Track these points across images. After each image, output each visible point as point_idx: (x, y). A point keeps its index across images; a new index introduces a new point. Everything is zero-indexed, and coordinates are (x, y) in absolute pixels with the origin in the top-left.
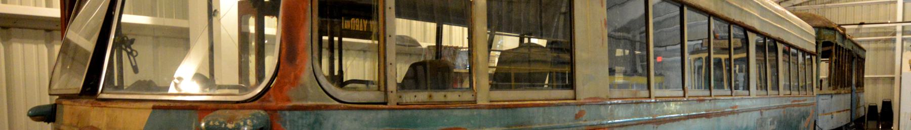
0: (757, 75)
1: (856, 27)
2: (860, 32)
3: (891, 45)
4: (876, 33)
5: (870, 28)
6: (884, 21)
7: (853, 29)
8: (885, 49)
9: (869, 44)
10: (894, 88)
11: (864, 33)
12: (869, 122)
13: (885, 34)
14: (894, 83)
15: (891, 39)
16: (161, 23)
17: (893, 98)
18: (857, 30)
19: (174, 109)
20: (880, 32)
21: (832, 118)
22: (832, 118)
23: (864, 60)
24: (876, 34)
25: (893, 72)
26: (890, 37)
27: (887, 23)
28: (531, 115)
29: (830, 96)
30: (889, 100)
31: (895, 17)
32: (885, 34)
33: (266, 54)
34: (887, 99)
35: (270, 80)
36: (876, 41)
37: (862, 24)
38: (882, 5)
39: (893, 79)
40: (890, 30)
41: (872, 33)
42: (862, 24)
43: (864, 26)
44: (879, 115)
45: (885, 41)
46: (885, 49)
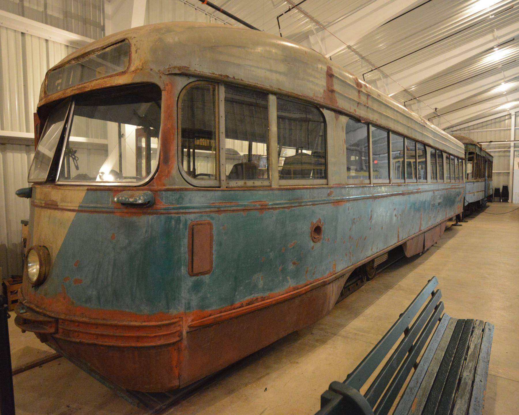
1: (488, 143)
2: (490, 146)
3: (508, 154)
5: (495, 144)
7: (486, 145)
8: (504, 156)
10: (509, 178)
13: (504, 147)
17: (509, 184)
18: (489, 145)
20: (501, 147)
24: (499, 148)
25: (509, 169)
26: (507, 149)
31: (510, 138)
32: (504, 147)
33: (151, 159)
34: (505, 184)
36: (499, 152)
37: (491, 142)
39: (509, 173)
41: (497, 147)
42: (491, 142)
43: (492, 143)
44: (501, 194)
45: (505, 151)
46: (504, 156)
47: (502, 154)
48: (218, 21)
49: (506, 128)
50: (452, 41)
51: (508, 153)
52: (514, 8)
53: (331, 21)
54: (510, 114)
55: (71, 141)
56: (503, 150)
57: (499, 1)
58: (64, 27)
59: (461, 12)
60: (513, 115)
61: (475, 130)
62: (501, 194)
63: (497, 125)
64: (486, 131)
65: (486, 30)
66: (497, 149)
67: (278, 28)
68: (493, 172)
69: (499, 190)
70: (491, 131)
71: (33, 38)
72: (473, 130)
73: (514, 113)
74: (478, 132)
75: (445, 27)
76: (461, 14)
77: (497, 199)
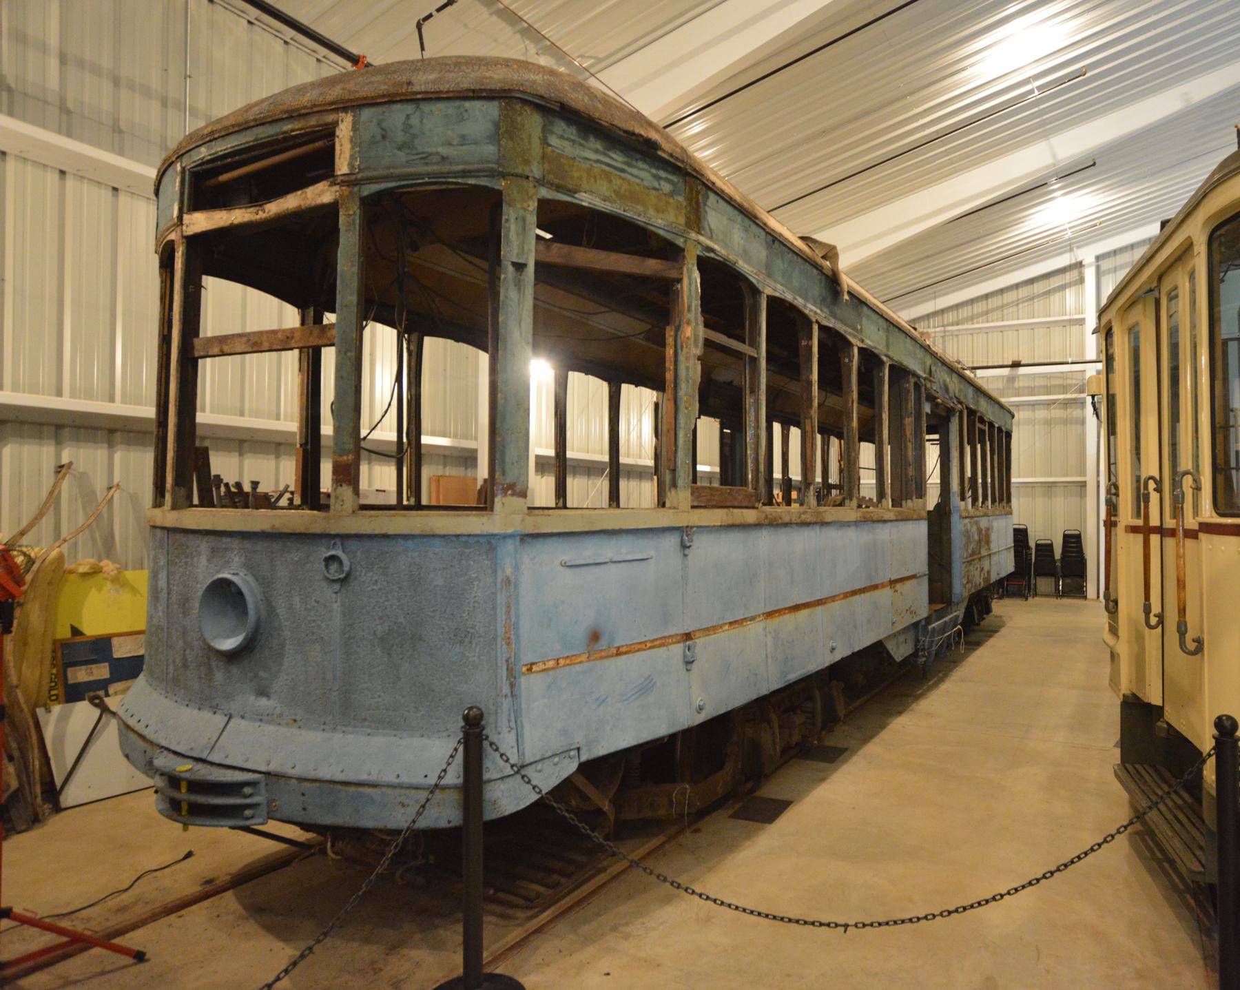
0: (301, 410)
1: (1006, 371)
2: (1016, 385)
3: (1076, 413)
4: (1047, 387)
5: (1034, 376)
6: (1061, 360)
7: (1002, 377)
8: (1066, 422)
9: (1034, 411)
10: (1085, 504)
11: (1024, 387)
12: (1039, 579)
13: (1064, 389)
14: (1085, 495)
15: (1075, 399)
16: (457, 445)
17: (1085, 528)
18: (1011, 379)
19: (180, 532)
20: (1055, 386)
21: (689, 663)
22: (689, 663)
23: (1009, 435)
24: (1048, 390)
25: (1083, 472)
26: (1074, 396)
27: (1067, 363)
28: (410, 553)
29: (672, 541)
30: (1050, 542)
31: (1082, 351)
32: (1064, 389)
33: (423, 462)
34: (1072, 529)
35: (1148, 512)
36: (1049, 404)
37: (1016, 365)
38: (1057, 328)
39: (1083, 485)
40: (1074, 382)
41: (1040, 387)
42: (1016, 365)
43: (1022, 370)
44: (1058, 564)
45: (1066, 404)
46: (1066, 422)
47: (1057, 413)
48: (323, 65)
49: (1067, 317)
50: (952, 163)
51: (1079, 411)
52: (1087, 75)
53: (602, 55)
54: (1081, 263)
55: (203, 425)
56: (1062, 397)
57: (1056, 50)
58: (60, 126)
59: (1023, 222)
60: (1090, 265)
61: (963, 324)
62: (1058, 564)
63: (1038, 304)
64: (1002, 329)
65: (1029, 130)
66: (1039, 394)
67: (419, 47)
68: (1013, 480)
69: (1052, 551)
70: (1017, 328)
71: (70, 183)
72: (958, 324)
73: (1093, 259)
74: (972, 333)
75: (925, 111)
76: (1022, 225)
77: (1044, 584)
